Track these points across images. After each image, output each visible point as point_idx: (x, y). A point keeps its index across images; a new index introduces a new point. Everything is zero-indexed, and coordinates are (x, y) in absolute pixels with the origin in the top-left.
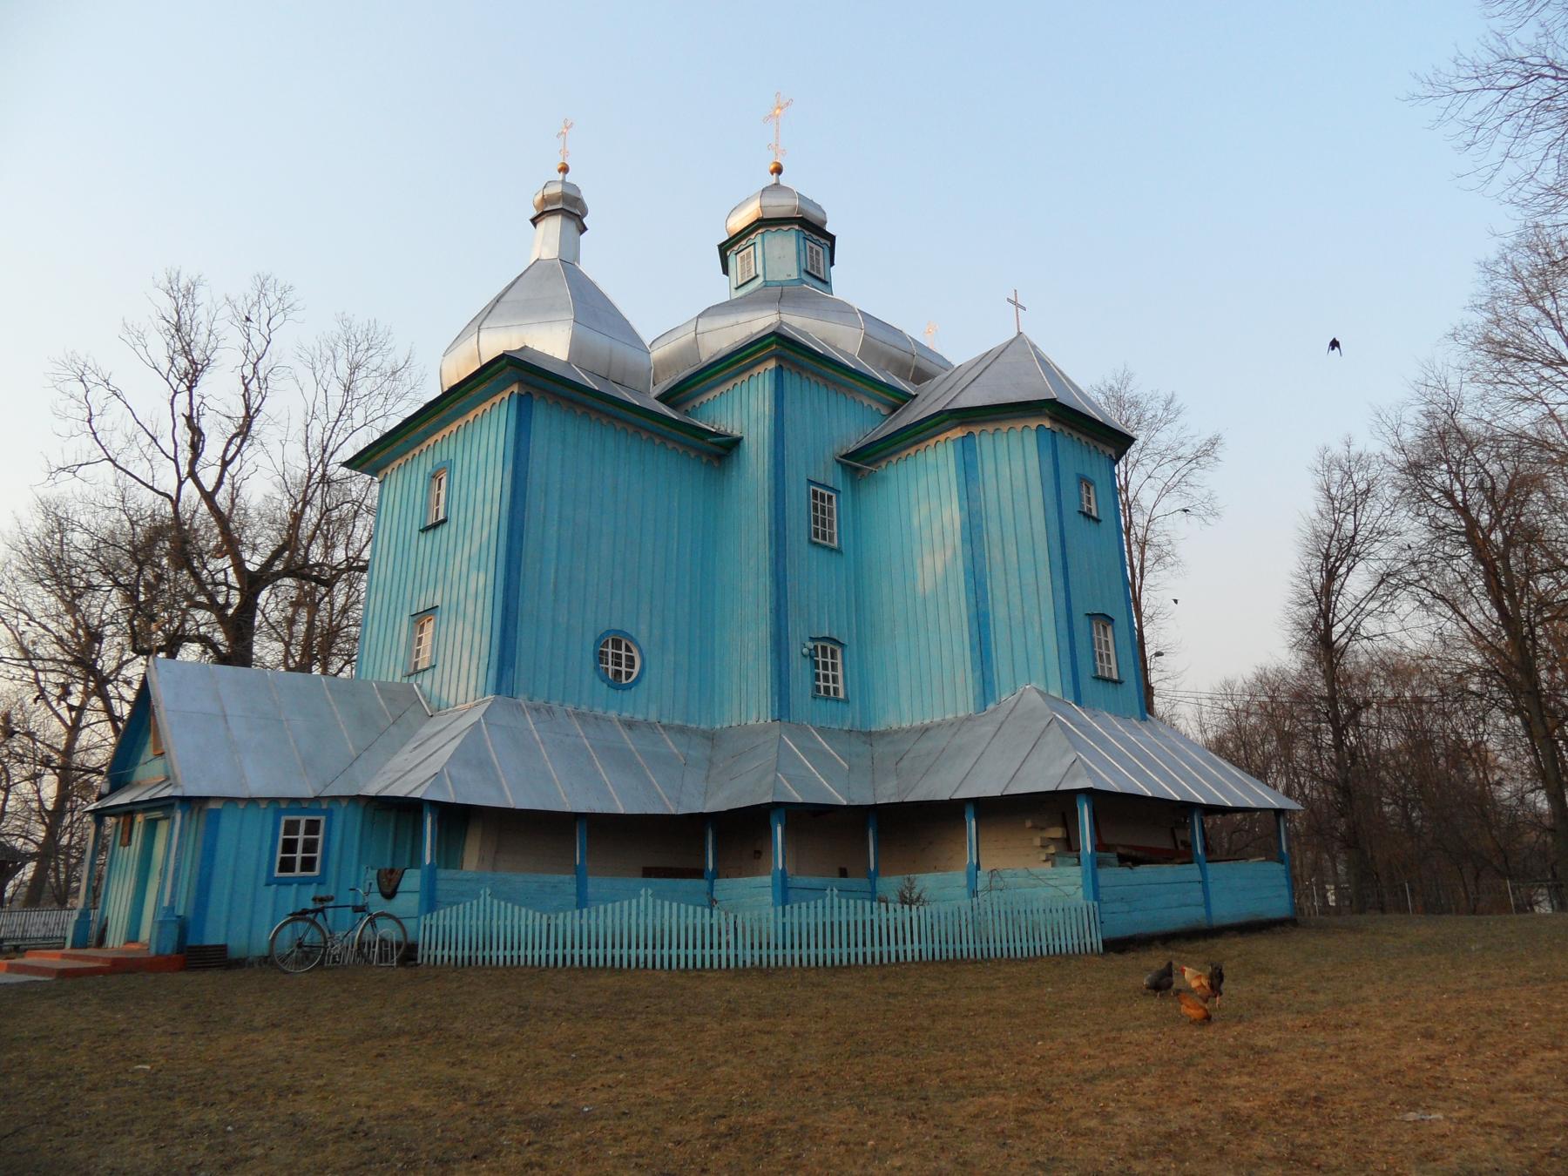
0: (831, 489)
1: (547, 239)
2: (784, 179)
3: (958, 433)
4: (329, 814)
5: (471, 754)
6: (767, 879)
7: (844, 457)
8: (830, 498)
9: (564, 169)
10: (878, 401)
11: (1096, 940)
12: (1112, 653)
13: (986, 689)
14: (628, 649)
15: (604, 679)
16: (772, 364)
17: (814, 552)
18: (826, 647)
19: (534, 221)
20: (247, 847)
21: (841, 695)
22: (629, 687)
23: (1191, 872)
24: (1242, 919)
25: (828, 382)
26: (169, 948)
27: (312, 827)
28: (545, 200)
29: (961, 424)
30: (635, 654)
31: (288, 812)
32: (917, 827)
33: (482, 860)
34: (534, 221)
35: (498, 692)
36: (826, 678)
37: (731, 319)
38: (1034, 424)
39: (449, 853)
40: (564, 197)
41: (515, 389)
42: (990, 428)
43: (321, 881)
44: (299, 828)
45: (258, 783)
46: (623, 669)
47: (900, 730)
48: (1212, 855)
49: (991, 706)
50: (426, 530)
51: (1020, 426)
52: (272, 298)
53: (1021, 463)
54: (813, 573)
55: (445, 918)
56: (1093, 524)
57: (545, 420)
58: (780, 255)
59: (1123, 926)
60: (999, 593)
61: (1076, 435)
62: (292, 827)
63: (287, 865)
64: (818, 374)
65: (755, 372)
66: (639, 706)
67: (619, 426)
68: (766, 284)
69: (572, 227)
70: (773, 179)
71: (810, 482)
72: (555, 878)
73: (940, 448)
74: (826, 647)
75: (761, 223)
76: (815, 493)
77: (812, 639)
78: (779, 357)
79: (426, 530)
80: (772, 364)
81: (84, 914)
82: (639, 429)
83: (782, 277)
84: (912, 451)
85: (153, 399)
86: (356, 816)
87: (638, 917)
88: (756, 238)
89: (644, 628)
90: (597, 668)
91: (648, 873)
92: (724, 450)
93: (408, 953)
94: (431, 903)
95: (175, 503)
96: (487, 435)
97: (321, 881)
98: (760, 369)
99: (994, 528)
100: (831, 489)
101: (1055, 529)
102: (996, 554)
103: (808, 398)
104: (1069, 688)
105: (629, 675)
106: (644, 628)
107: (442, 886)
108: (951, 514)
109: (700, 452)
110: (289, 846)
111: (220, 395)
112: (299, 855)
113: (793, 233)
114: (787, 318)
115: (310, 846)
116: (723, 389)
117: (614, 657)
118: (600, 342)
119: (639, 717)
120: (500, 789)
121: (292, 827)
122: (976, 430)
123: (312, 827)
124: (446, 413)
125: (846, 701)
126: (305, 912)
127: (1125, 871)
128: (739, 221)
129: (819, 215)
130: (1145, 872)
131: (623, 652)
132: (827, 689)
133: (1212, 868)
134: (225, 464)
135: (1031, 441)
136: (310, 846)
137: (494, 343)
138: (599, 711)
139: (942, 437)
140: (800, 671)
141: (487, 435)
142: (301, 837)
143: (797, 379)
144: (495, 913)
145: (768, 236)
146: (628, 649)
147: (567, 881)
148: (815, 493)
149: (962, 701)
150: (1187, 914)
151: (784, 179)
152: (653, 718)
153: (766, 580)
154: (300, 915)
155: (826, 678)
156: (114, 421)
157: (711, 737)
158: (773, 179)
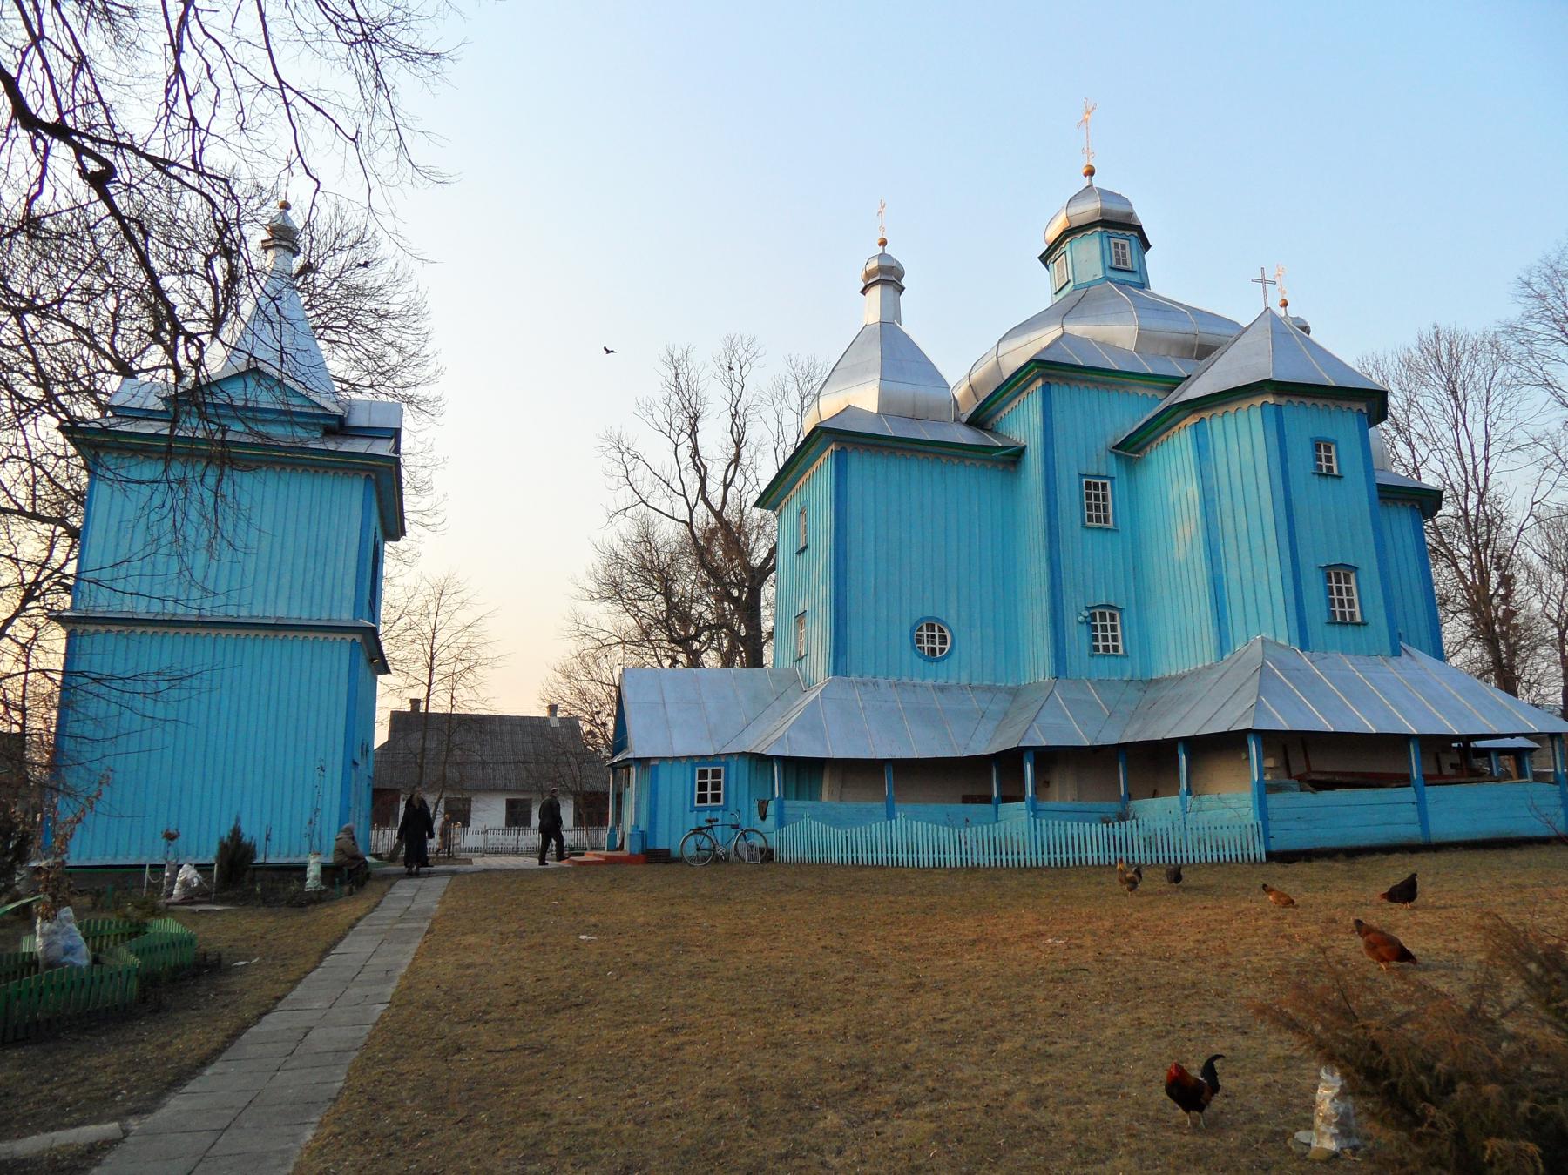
0: (1106, 477)
1: (871, 308)
2: (1097, 181)
3: (1191, 420)
4: (727, 765)
5: (811, 723)
6: (1023, 804)
7: (1116, 447)
8: (1104, 485)
9: (883, 243)
10: (1156, 388)
11: (1260, 851)
12: (1355, 598)
13: (1223, 641)
14: (941, 630)
15: (921, 656)
16: (1039, 383)
17: (1088, 534)
18: (1101, 617)
19: (864, 292)
20: (677, 788)
21: (1121, 651)
22: (942, 659)
23: (1406, 794)
24: (1479, 837)
25: (1098, 385)
26: (637, 850)
27: (716, 774)
28: (868, 275)
29: (1193, 412)
30: (947, 633)
31: (698, 765)
32: (1154, 763)
33: (831, 793)
34: (864, 292)
35: (835, 674)
36: (1105, 638)
37: (1024, 339)
38: (1258, 402)
39: (1042, 783)
40: (881, 269)
41: (833, 447)
42: (1219, 411)
43: (725, 809)
44: (708, 777)
45: (681, 748)
46: (937, 646)
47: (1171, 678)
48: (1430, 780)
49: (1227, 656)
50: (799, 553)
51: (1245, 405)
52: (741, 352)
53: (1248, 439)
54: (1091, 555)
55: (791, 831)
56: (1336, 481)
57: (859, 465)
58: (1088, 255)
59: (1289, 839)
60: (1232, 557)
61: (1320, 403)
62: (703, 774)
63: (702, 799)
64: (1082, 381)
65: (1030, 390)
66: (952, 672)
67: (921, 456)
68: (1076, 288)
69: (890, 290)
70: (1086, 181)
71: (1082, 476)
72: (870, 805)
73: (1242, 416)
74: (1101, 617)
75: (1069, 233)
76: (1088, 484)
77: (1087, 608)
78: (1043, 376)
79: (799, 553)
80: (1039, 383)
81: (613, 830)
82: (938, 456)
83: (1089, 279)
84: (1164, 437)
85: (660, 453)
86: (744, 765)
87: (919, 831)
88: (1066, 246)
89: (953, 613)
90: (913, 648)
91: (966, 799)
92: (1014, 457)
93: (767, 855)
94: (781, 823)
95: (689, 525)
96: (819, 483)
97: (725, 809)
98: (1033, 387)
99: (1226, 501)
100: (1106, 477)
101: (1280, 494)
102: (1228, 522)
103: (1074, 403)
104: (1295, 635)
105: (942, 650)
106: (953, 613)
107: (788, 811)
108: (1193, 490)
109: (995, 462)
110: (703, 786)
111: (714, 441)
112: (709, 792)
113: (1097, 236)
114: (1069, 329)
115: (716, 786)
116: (1012, 405)
117: (929, 639)
118: (906, 390)
119: (952, 682)
120: (825, 746)
121: (703, 774)
122: (1206, 415)
123: (716, 774)
124: (799, 466)
125: (1126, 655)
126: (700, 829)
127: (1309, 798)
128: (1054, 232)
129: (1125, 209)
130: (1327, 796)
131: (937, 633)
132: (1106, 648)
133: (1432, 792)
134: (726, 487)
135: (1256, 416)
136: (716, 786)
137: (828, 407)
138: (917, 681)
139: (1182, 425)
140: (1078, 637)
141: (819, 483)
142: (709, 780)
143: (1066, 389)
144: (816, 830)
145: (1075, 243)
146: (941, 630)
147: (879, 807)
148: (1088, 484)
149: (1205, 654)
150: (1405, 828)
151: (1097, 181)
152: (964, 681)
153: (1044, 564)
154: (698, 830)
155: (1105, 638)
156: (639, 473)
157: (1015, 693)
158: (1086, 181)
